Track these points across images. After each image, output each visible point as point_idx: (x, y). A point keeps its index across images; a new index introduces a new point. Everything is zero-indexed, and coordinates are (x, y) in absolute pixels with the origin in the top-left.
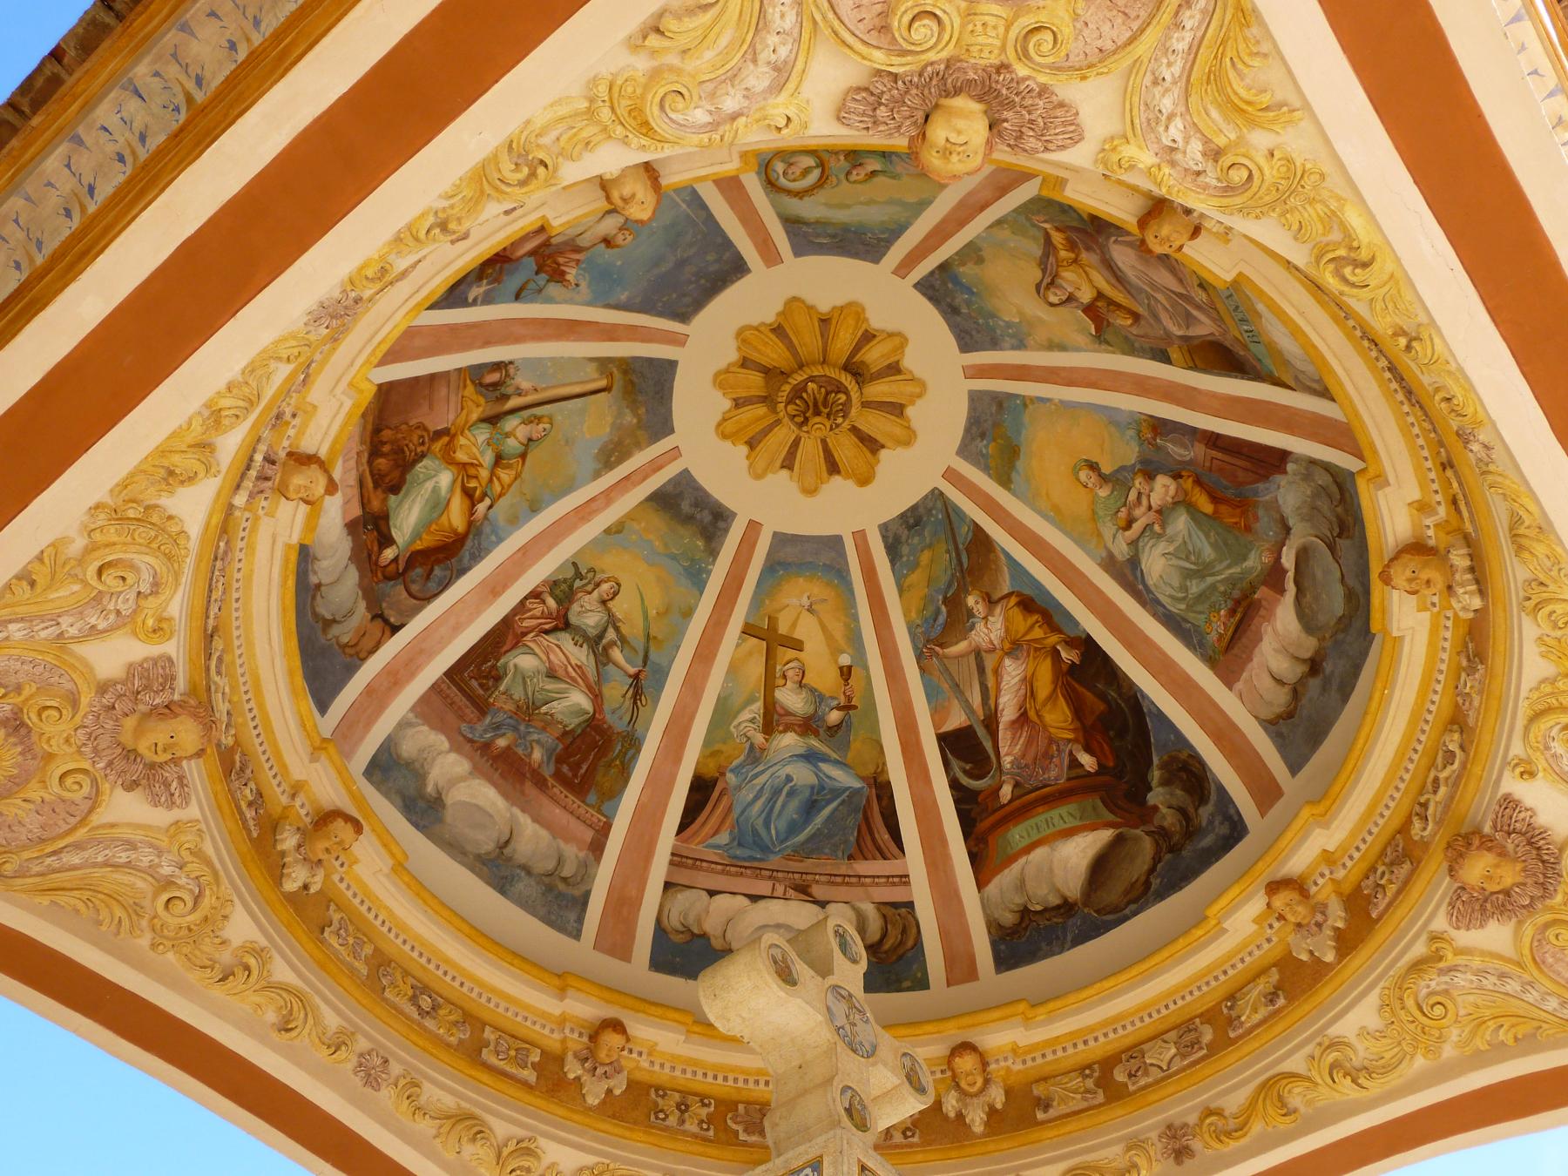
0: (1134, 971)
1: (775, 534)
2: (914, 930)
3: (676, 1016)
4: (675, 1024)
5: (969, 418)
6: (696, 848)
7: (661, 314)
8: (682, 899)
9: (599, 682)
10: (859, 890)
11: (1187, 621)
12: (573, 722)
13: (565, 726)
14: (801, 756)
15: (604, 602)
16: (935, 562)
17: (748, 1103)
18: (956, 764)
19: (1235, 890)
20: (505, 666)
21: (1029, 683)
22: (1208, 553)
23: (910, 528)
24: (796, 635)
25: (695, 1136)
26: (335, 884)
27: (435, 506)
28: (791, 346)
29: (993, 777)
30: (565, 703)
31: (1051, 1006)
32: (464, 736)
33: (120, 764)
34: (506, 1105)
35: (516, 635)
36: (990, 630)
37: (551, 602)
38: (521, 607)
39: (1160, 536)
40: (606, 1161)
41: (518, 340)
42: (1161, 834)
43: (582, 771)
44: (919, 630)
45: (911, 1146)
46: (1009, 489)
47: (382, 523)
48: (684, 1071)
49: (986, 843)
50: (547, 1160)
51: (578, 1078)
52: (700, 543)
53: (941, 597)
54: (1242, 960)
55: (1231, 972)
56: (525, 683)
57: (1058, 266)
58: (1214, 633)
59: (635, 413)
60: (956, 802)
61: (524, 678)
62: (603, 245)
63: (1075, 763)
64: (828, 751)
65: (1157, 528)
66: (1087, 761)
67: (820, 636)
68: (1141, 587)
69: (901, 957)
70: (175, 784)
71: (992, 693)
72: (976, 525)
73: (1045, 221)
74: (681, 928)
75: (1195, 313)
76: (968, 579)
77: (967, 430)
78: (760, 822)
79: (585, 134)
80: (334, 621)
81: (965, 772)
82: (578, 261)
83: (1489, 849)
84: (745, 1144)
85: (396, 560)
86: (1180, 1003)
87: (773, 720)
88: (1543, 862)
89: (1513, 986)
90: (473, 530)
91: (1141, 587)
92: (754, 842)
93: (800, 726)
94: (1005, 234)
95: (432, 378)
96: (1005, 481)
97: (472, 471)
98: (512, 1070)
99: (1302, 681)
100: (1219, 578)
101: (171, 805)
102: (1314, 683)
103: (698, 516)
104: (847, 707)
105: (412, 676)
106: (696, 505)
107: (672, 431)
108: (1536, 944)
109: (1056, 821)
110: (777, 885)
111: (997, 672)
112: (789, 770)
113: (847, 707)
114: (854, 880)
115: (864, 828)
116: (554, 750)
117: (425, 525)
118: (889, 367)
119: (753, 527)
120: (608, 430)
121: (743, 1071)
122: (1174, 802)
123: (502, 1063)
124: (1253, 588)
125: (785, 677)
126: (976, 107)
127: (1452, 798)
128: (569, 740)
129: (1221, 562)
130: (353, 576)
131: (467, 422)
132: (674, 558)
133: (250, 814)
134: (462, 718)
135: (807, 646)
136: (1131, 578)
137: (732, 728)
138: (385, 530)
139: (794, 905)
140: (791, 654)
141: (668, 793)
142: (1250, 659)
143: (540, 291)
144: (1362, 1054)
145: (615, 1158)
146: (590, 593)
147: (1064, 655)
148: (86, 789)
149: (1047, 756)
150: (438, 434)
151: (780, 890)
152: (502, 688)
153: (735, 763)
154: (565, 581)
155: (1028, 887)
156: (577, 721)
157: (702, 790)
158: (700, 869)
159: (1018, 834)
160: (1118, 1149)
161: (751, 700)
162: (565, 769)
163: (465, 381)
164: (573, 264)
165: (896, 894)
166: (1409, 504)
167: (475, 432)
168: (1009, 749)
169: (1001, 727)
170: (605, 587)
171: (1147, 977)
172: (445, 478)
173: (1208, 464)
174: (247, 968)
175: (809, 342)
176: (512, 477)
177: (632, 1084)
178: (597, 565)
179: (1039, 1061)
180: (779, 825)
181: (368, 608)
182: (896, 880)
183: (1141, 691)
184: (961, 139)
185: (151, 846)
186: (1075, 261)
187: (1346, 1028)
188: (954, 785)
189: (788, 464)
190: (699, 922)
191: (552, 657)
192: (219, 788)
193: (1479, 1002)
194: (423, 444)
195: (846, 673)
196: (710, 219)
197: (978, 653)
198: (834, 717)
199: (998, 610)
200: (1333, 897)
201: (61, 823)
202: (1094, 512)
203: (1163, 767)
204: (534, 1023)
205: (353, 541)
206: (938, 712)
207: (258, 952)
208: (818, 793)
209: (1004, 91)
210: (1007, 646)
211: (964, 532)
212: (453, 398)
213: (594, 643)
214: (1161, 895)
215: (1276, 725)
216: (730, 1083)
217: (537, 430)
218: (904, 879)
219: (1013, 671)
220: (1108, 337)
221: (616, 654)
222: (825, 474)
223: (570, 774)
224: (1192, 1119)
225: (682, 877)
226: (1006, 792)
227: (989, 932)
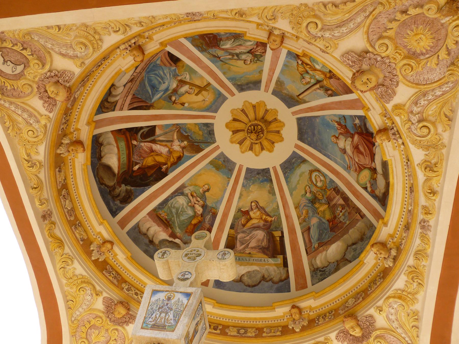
0: (91, 195)
2: (107, 111)
5: (230, 159)
7: (305, 117)
10: (124, 96)
13: (223, 41)
14: (168, 87)
16: (198, 135)
18: (146, 130)
19: (111, 230)
21: (160, 154)
22: (182, 218)
23: (210, 131)
24: (200, 95)
29: (140, 139)
31: (86, 170)
36: (177, 146)
39: (188, 204)
41: (332, 103)
42: (113, 188)
46: (209, 163)
49: (123, 135)
52: (239, 83)
53: (189, 134)
54: (89, 226)
55: (86, 223)
57: (261, 212)
60: (137, 128)
63: (137, 164)
64: (166, 95)
65: (190, 204)
66: (136, 168)
68: (176, 194)
71: (161, 143)
72: (203, 150)
75: (243, 246)
76: (191, 143)
77: (227, 157)
78: (157, 72)
81: (144, 132)
86: (79, 207)
87: (182, 83)
91: (176, 194)
94: (274, 206)
96: (211, 163)
99: (148, 237)
100: (175, 219)
102: (147, 241)
103: (246, 86)
104: (174, 102)
109: (123, 156)
111: (166, 146)
112: (167, 83)
115: (140, 100)
118: (252, 148)
120: (287, 88)
122: (121, 193)
124: (171, 228)
125: (191, 89)
127: (134, 299)
129: (179, 221)
132: (241, 77)
135: (196, 96)
136: (179, 192)
140: (196, 92)
142: (154, 222)
147: (165, 166)
149: (141, 156)
153: (177, 70)
159: (123, 144)
160: (46, 196)
161: (191, 78)
164: (339, 128)
168: (145, 145)
169: (152, 144)
170: (249, 62)
171: (137, 269)
173: (204, 226)
175: (272, 137)
180: (152, 76)
186: (261, 218)
187: (76, 264)
188: (142, 128)
193: (81, 298)
195: (183, 104)
196: (320, 152)
197: (172, 141)
198: (173, 98)
199: (181, 150)
201: (374, 27)
203: (131, 190)
206: (161, 127)
210: (171, 150)
211: (203, 146)
214: (100, 189)
215: (137, 227)
218: (121, 109)
219: (164, 150)
220: (240, 213)
222: (234, 117)
224: (53, 219)
226: (135, 143)
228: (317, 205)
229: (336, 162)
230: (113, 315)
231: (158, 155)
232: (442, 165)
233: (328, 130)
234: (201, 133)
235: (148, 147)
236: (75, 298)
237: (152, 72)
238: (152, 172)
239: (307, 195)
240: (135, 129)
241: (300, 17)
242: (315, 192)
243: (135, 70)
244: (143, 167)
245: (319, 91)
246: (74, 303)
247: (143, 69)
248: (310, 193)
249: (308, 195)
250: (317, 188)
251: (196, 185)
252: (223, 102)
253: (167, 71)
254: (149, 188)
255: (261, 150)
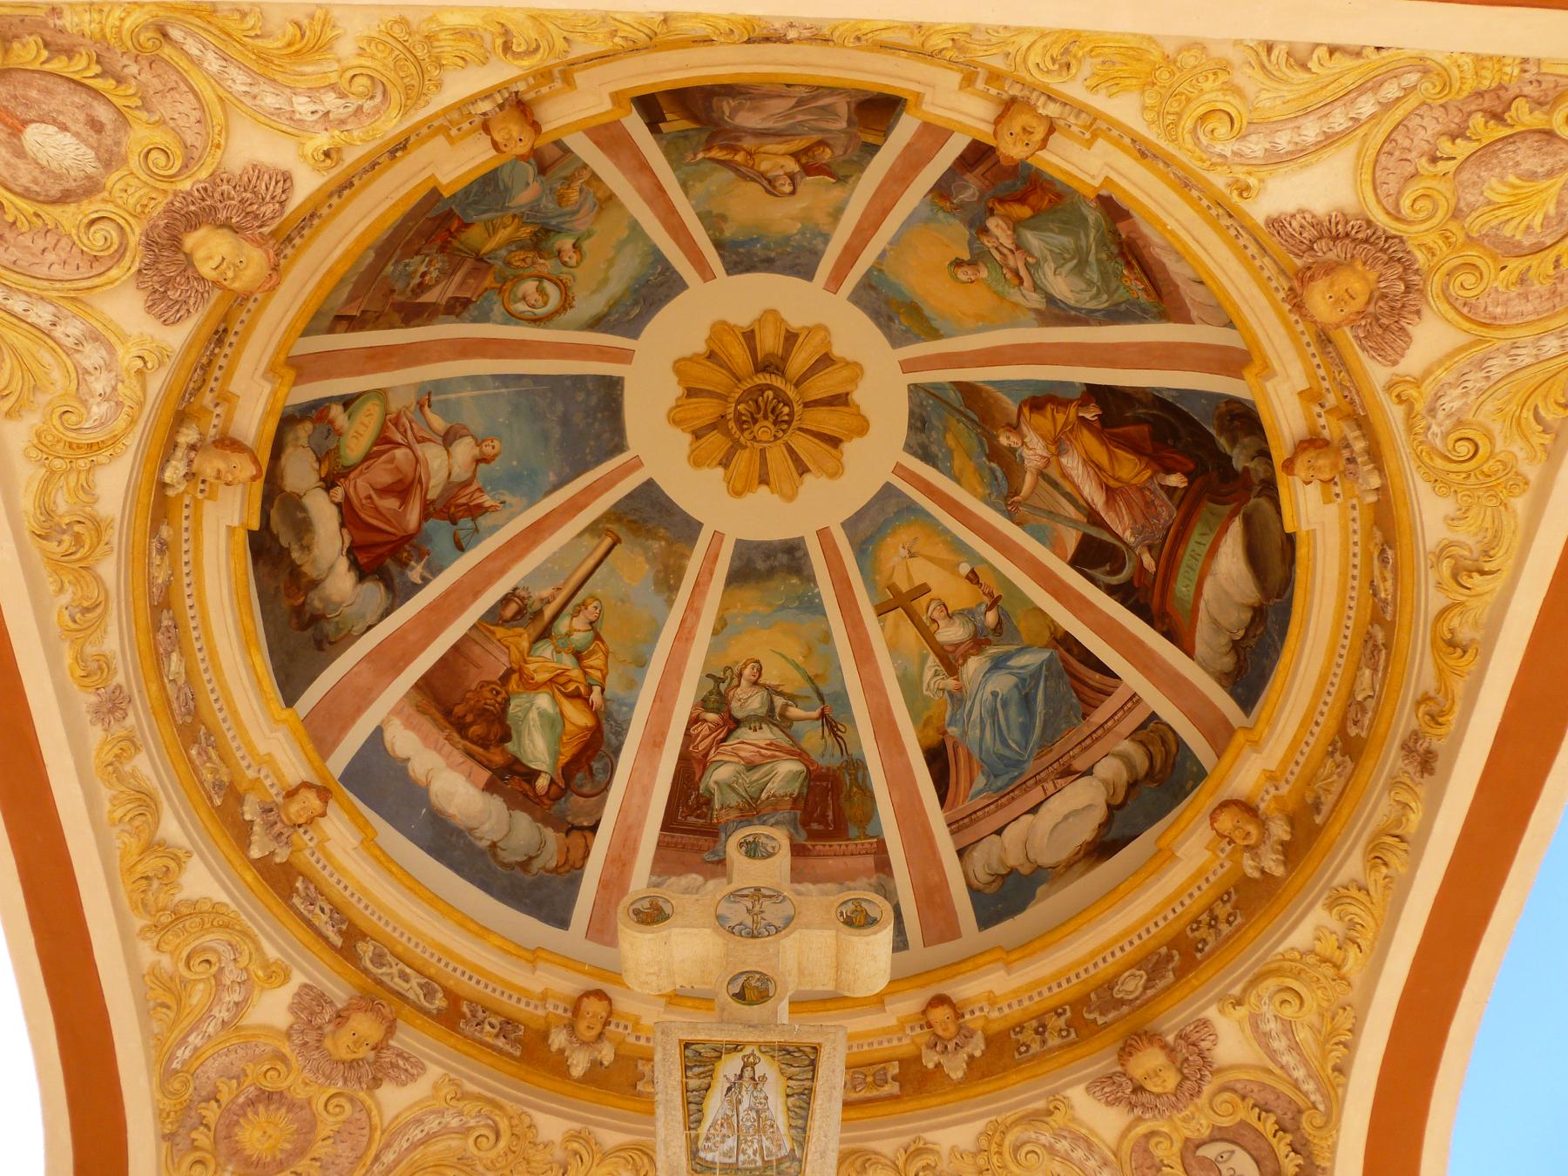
1: (843, 525)
2: (1170, 735)
3: (987, 958)
4: (991, 966)
6: (964, 806)
7: (598, 462)
8: (978, 855)
9: (795, 743)
11: (1119, 304)
12: (795, 788)
13: (791, 795)
14: (990, 670)
15: (755, 683)
16: (958, 437)
17: (1095, 990)
20: (708, 789)
21: (1089, 462)
22: (1067, 241)
23: (923, 430)
24: (917, 584)
25: (1061, 1047)
26: (634, 1045)
27: (553, 724)
28: (711, 394)
30: (778, 779)
32: (712, 862)
33: (352, 1074)
34: (882, 1125)
35: (699, 761)
36: (1033, 449)
37: (711, 716)
38: (688, 737)
39: (1038, 263)
40: (993, 1118)
41: (502, 572)
43: (831, 818)
44: (993, 497)
45: (1239, 928)
47: (517, 767)
48: (1031, 998)
50: (945, 1149)
51: (938, 1066)
52: (795, 581)
56: (734, 789)
57: (752, 168)
58: (1140, 293)
59: (656, 537)
60: (1123, 602)
61: (730, 786)
62: (482, 466)
63: (1171, 491)
66: (1175, 480)
67: (933, 567)
68: (1073, 313)
69: (1174, 764)
70: (401, 1063)
73: (695, 155)
74: (991, 879)
77: (879, 325)
78: (998, 745)
79: (72, 484)
80: (531, 859)
82: (479, 489)
83: (1312, 278)
84: (1106, 1025)
85: (552, 782)
87: (950, 661)
88: (1366, 241)
89: (1499, 365)
90: (602, 717)
91: (1073, 313)
92: (1006, 766)
93: (972, 648)
95: (456, 648)
96: (935, 334)
97: (562, 680)
98: (875, 1093)
100: (1093, 251)
101: (413, 1078)
103: (777, 563)
105: (634, 851)
106: (768, 557)
107: (700, 525)
108: (1465, 310)
110: (1045, 785)
111: (1065, 476)
113: (995, 602)
114: (1100, 732)
115: (1077, 685)
116: (795, 819)
117: (556, 744)
118: (786, 339)
119: (824, 534)
120: (647, 567)
121: (1079, 963)
123: (862, 1094)
124: (1116, 233)
125: (934, 621)
126: (202, 232)
128: (802, 804)
130: (523, 820)
131: (521, 652)
132: (783, 607)
133: (500, 1042)
134: (700, 850)
135: (932, 584)
137: (925, 693)
138: (522, 770)
139: (1068, 790)
140: (924, 600)
141: (914, 783)
142: (1177, 286)
143: (477, 530)
144: (1471, 542)
145: (999, 1111)
146: (738, 686)
147: (1088, 416)
148: (348, 1107)
149: (1149, 504)
150: (505, 678)
151: (1050, 787)
152: (717, 806)
153: (947, 717)
154: (711, 693)
155: (1222, 622)
156: (797, 785)
157: (938, 758)
158: (978, 820)
159: (1182, 586)
162: (815, 826)
163: (489, 630)
165: (1136, 718)
166: (961, 88)
167: (538, 653)
168: (1122, 526)
169: (1103, 514)
170: (747, 672)
172: (543, 701)
173: (987, 183)
174: (576, 1153)
175: (715, 378)
176: (602, 657)
177: (989, 1041)
178: (728, 662)
179: (1297, 770)
180: (1013, 737)
181: (557, 829)
182: (1130, 705)
183: (1153, 389)
184: (217, 260)
185: (433, 1112)
188: (1111, 591)
189: (803, 470)
190: (1002, 862)
191: (742, 754)
192: (453, 1041)
193: (1498, 404)
194: (498, 693)
195: (973, 577)
196: (536, 379)
197: (1042, 474)
198: (991, 618)
199: (1024, 429)
200: (1343, 425)
202: (996, 293)
204: (880, 1043)
205: (500, 795)
206: (1055, 546)
207: (576, 1136)
208: (1024, 687)
209: (192, 208)
210: (1053, 448)
211: (954, 396)
212: (490, 647)
213: (771, 717)
216: (1074, 981)
217: (591, 612)
218: (1135, 699)
219: (1072, 463)
221: (794, 712)
222: (833, 451)
223: (822, 827)
225: (967, 837)
226: (1148, 560)
227: (1223, 687)
228: (525, 232)
229: (476, 381)
230: (1382, 285)
231: (1097, 466)
232: (130, 898)
233: (515, 463)
234: (951, 442)
235: (1115, 511)
236: (1519, 424)
237: (1009, 759)
238: (1131, 429)
239: (573, 241)
240: (1131, 601)
241: (514, 1152)
242: (542, 261)
243: (1042, 803)
244: (1157, 468)
245: (545, 593)
246: (1537, 399)
247: (1024, 787)
248: (559, 252)
249: (566, 243)
250: (536, 272)
251: (1001, 297)
252: (860, 515)
253: (973, 736)
254: (1160, 390)
255: (757, 332)
